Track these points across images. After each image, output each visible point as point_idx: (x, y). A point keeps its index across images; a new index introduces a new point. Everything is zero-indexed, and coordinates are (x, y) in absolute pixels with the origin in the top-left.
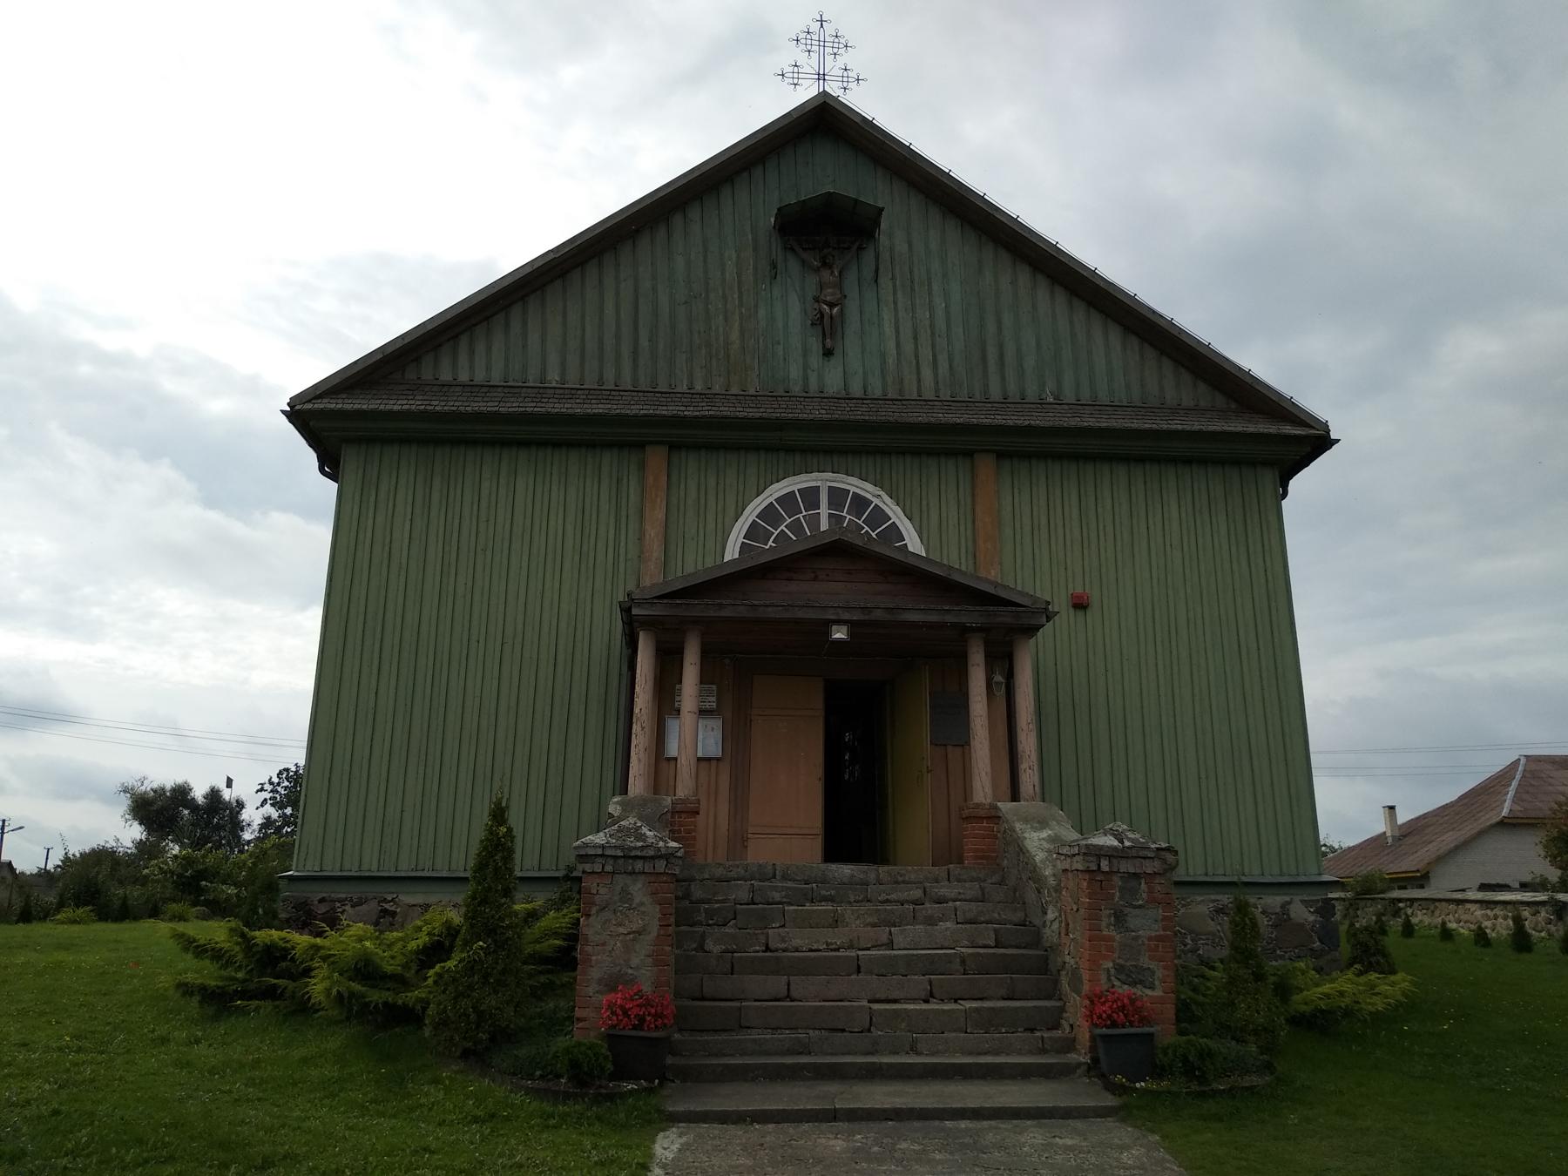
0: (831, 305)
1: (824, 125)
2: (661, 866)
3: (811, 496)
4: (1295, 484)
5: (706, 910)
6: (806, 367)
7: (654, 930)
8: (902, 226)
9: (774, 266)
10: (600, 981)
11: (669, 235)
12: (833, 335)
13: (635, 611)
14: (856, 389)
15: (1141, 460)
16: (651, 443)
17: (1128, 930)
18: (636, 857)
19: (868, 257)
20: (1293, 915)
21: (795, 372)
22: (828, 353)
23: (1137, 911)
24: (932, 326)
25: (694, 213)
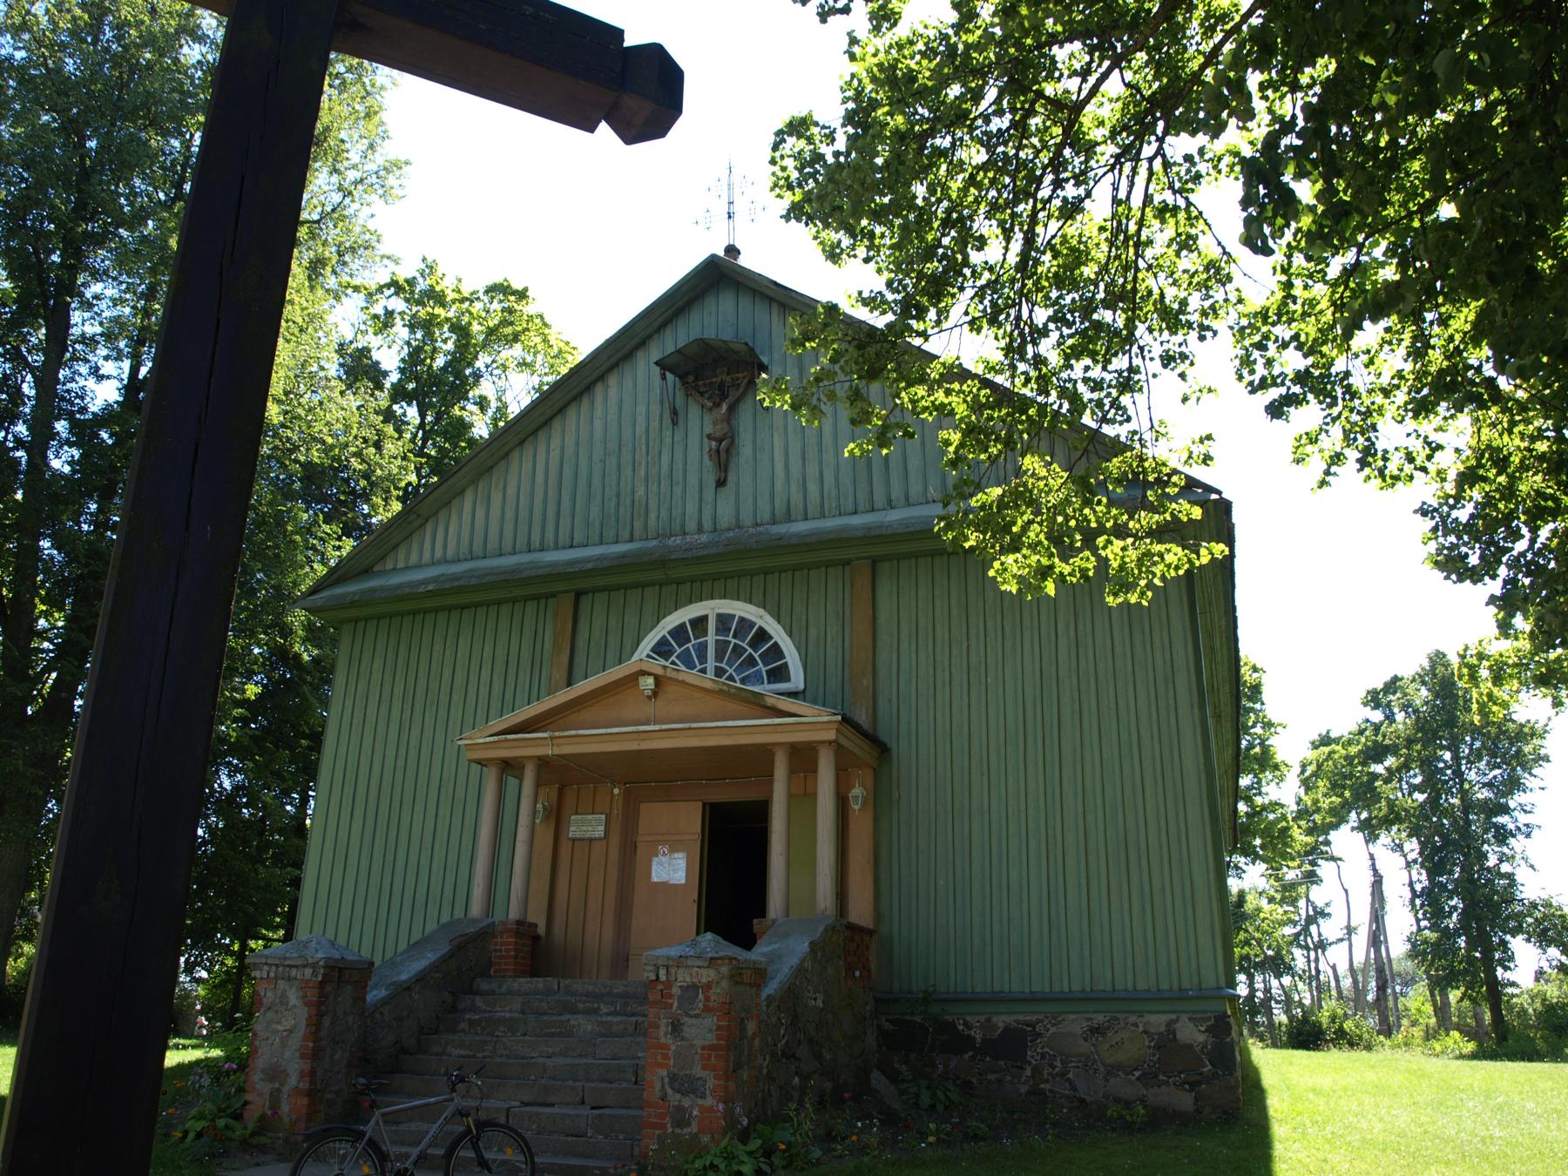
3: (699, 623)
9: (675, 413)
17: (683, 1039)
18: (290, 966)
20: (1179, 1036)
23: (694, 1021)
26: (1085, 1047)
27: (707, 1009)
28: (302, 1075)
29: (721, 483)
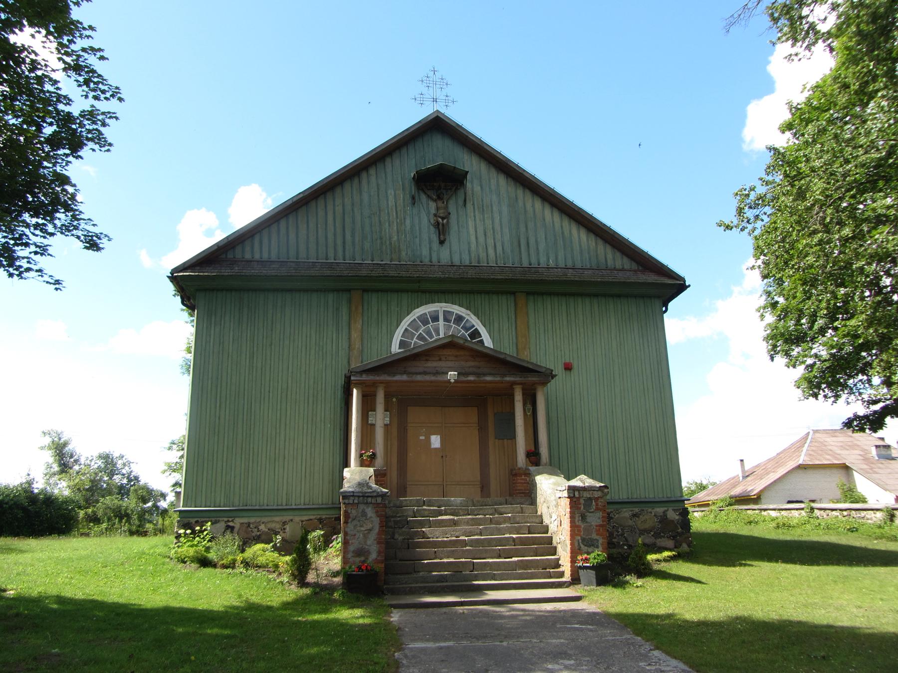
0: (443, 219)
1: (438, 126)
2: (379, 500)
4: (670, 305)
5: (394, 521)
6: (430, 249)
7: (377, 529)
8: (480, 180)
9: (413, 198)
10: (353, 552)
11: (360, 182)
12: (444, 235)
13: (352, 378)
14: (457, 261)
15: (596, 295)
16: (354, 289)
18: (368, 497)
19: (461, 193)
21: (425, 252)
22: (442, 242)
24: (493, 228)
25: (372, 171)
26: (630, 523)
27: (597, 509)
28: (379, 553)
29: (442, 242)
